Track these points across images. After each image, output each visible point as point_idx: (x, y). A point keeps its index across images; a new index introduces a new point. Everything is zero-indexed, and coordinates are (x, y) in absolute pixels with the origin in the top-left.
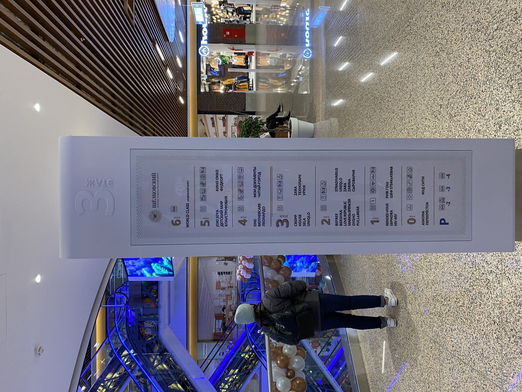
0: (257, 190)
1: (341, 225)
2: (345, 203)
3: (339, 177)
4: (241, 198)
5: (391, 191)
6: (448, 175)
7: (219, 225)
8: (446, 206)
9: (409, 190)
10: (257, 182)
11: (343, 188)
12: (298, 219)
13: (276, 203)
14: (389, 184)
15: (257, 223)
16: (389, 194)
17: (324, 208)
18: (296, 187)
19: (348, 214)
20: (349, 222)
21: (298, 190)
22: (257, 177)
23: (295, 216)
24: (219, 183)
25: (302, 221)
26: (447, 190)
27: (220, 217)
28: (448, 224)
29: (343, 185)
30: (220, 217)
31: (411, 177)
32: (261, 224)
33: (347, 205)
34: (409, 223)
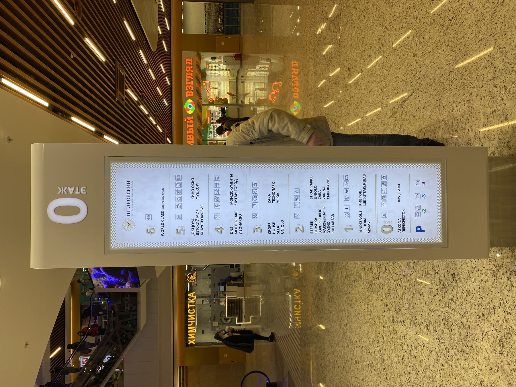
0: (234, 197)
1: (316, 233)
2: (320, 211)
3: (313, 185)
4: (217, 206)
5: (365, 199)
6: (424, 183)
7: (195, 234)
8: (422, 213)
9: (384, 197)
10: (233, 189)
11: (318, 195)
12: (272, 227)
13: (252, 211)
14: (362, 191)
15: (234, 231)
16: (362, 202)
17: (297, 216)
18: (269, 195)
19: (323, 221)
20: (325, 229)
21: (271, 198)
22: (234, 184)
23: (269, 224)
24: (195, 191)
25: (276, 229)
26: (422, 198)
27: (195, 225)
28: (424, 231)
29: (318, 193)
30: (195, 225)
31: (385, 185)
32: (238, 231)
33: (322, 213)
34: (383, 231)
